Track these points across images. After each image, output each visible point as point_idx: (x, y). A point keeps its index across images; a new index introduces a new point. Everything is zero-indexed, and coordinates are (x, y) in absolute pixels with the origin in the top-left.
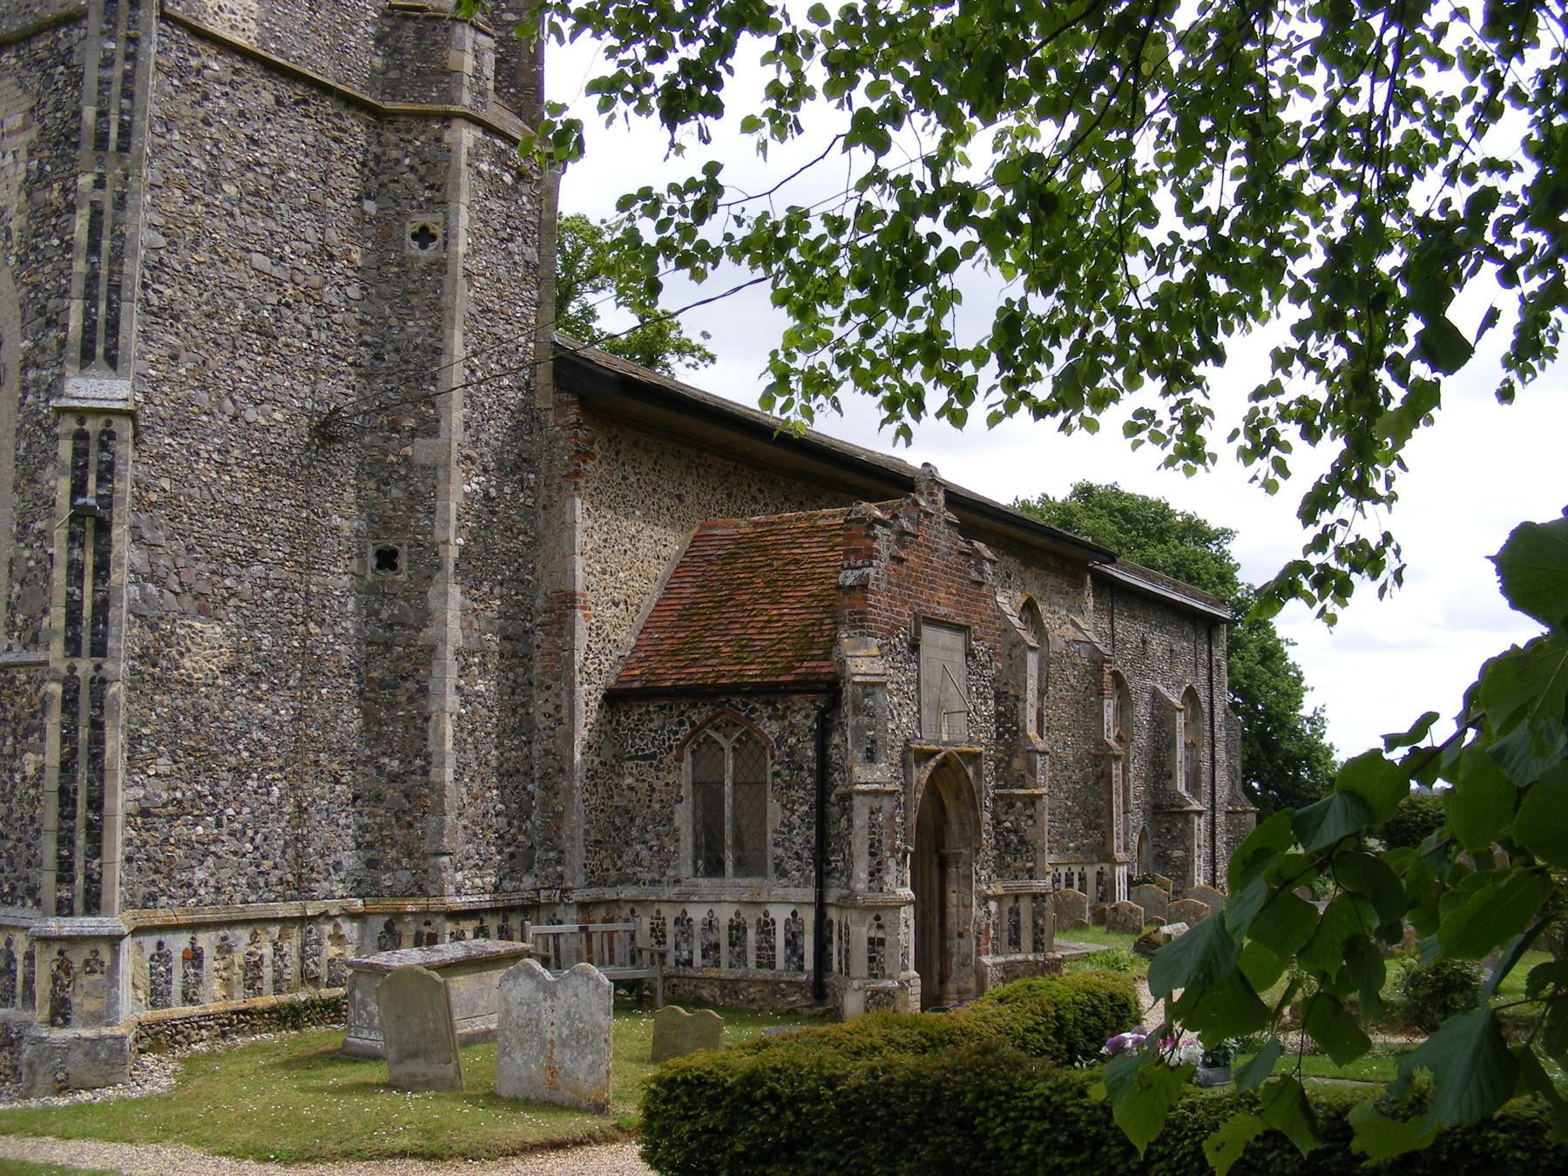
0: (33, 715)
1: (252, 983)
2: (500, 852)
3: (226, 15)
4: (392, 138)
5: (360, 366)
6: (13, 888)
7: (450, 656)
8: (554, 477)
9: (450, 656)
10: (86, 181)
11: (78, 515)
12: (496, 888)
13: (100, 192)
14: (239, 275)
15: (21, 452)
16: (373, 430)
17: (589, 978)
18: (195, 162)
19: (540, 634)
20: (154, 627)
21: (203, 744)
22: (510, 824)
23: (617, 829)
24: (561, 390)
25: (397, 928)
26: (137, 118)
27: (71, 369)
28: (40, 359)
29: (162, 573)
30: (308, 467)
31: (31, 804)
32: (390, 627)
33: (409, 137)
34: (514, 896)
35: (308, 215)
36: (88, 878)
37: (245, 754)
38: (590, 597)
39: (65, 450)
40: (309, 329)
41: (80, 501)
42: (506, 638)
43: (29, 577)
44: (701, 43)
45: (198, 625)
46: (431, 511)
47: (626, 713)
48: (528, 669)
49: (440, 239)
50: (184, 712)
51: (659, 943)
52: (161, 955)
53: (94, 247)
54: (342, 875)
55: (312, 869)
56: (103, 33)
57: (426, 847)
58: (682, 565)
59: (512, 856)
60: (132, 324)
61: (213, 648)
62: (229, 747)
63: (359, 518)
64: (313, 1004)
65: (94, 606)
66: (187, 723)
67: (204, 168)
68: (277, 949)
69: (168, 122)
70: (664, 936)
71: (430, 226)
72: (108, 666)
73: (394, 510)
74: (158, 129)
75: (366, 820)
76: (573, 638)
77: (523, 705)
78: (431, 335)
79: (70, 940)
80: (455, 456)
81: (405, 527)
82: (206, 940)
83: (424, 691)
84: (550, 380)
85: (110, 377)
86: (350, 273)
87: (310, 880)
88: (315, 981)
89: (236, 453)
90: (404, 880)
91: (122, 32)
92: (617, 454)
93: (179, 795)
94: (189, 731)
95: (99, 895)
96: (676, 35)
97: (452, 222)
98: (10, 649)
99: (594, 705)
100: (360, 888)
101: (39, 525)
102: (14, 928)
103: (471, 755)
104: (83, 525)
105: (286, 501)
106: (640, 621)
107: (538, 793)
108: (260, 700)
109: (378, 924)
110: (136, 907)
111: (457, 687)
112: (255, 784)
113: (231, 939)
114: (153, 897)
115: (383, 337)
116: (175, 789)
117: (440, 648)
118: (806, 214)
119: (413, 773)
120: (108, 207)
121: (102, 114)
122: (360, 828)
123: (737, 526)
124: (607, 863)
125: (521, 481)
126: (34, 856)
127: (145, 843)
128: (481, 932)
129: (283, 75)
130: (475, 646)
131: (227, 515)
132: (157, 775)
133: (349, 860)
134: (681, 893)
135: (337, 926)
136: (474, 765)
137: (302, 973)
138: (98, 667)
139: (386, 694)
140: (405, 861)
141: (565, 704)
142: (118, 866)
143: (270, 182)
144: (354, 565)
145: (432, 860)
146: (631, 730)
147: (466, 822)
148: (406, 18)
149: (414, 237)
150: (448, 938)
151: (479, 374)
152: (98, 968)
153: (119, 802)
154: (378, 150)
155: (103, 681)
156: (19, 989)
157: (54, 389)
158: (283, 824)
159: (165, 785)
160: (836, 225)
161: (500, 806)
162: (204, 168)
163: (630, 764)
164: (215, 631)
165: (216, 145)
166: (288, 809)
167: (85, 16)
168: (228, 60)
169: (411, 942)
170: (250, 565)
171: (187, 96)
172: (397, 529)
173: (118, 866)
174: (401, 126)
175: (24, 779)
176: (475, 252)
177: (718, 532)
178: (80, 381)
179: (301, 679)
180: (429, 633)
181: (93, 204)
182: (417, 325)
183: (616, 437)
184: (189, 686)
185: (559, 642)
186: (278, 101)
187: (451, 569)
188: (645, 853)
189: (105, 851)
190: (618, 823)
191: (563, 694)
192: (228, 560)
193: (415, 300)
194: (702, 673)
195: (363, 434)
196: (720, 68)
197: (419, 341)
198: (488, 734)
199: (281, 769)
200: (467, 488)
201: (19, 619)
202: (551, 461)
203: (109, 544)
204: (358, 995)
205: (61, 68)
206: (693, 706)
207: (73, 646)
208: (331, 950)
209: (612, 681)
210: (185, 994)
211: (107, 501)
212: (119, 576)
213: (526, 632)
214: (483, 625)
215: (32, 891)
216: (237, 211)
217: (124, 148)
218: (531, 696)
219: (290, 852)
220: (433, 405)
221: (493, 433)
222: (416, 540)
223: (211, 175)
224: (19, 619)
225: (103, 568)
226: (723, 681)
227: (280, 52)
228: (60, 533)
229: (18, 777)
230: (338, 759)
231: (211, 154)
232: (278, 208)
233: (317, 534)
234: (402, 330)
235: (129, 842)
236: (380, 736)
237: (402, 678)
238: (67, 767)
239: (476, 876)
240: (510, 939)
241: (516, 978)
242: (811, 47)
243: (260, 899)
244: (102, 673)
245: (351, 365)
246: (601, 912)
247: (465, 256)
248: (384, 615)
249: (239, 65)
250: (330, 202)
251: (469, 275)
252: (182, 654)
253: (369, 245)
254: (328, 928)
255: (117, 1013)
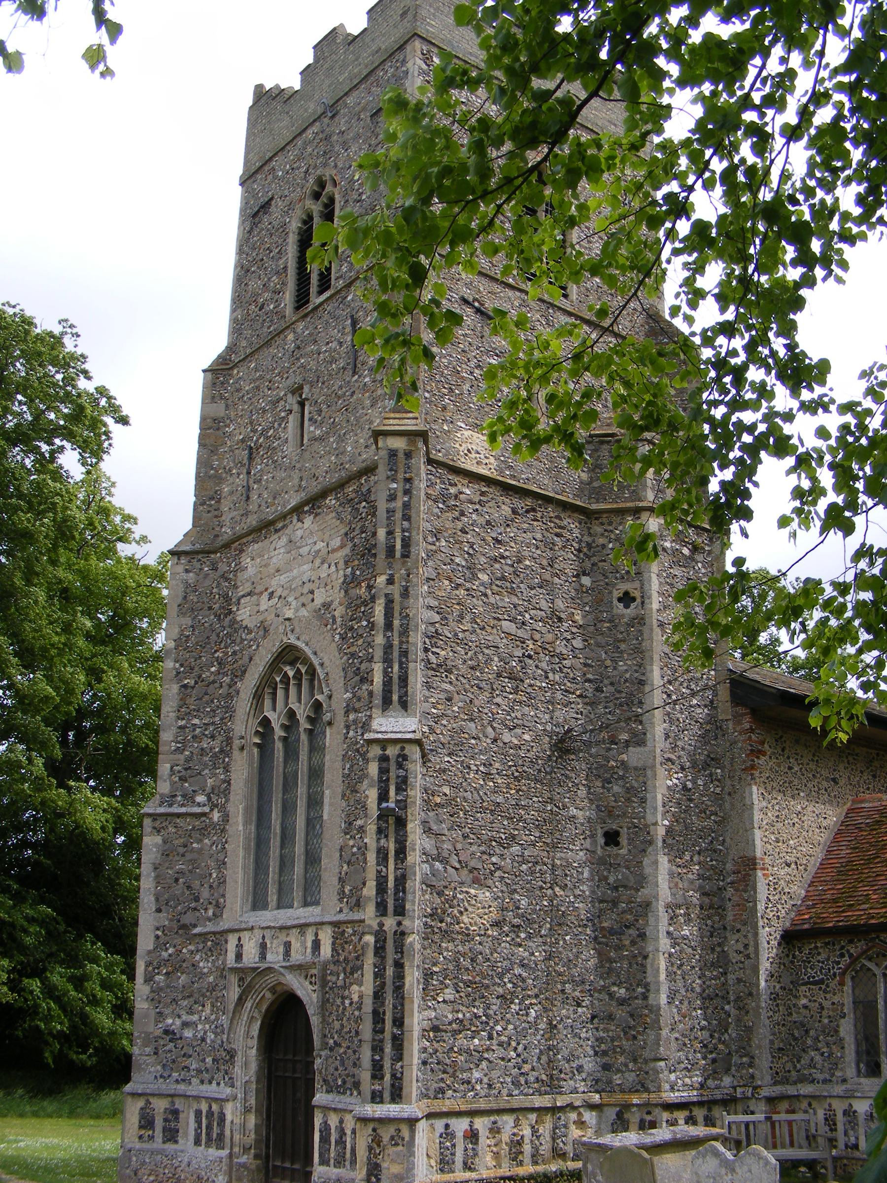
0: (357, 958)
1: (516, 1157)
2: (704, 1058)
3: (473, 455)
4: (599, 529)
5: (586, 697)
6: (344, 1082)
7: (661, 910)
8: (735, 771)
9: (661, 910)
10: (381, 580)
11: (383, 816)
12: (702, 1086)
13: (391, 587)
14: (494, 637)
15: (346, 771)
16: (598, 743)
17: (760, 1157)
18: (457, 560)
19: (730, 891)
20: (440, 894)
21: (478, 979)
22: (712, 1036)
23: (796, 1039)
24: (737, 705)
25: (625, 1116)
26: (414, 533)
27: (376, 712)
28: (357, 705)
29: (445, 854)
30: (550, 773)
31: (356, 1022)
32: (616, 888)
33: (611, 528)
34: (716, 1092)
35: (541, 591)
36: (393, 1076)
37: (509, 986)
38: (767, 860)
39: (373, 769)
40: (546, 672)
41: (384, 805)
42: (705, 894)
43: (354, 859)
44: (732, 468)
45: (472, 891)
46: (643, 801)
47: (800, 949)
48: (722, 917)
49: (639, 600)
50: (464, 955)
51: (831, 1130)
52: (448, 1134)
53: (389, 626)
54: (584, 1075)
55: (561, 1071)
56: (388, 478)
57: (647, 1054)
58: (839, 833)
59: (714, 1061)
60: (417, 677)
61: (484, 908)
62: (497, 980)
63: (590, 809)
64: (562, 1174)
65: (396, 879)
66: (466, 963)
67: (464, 563)
68: (534, 1131)
69: (437, 534)
70: (835, 1124)
71: (631, 591)
72: (406, 923)
73: (615, 801)
74: (430, 539)
75: (602, 1034)
76: (755, 892)
77: (719, 945)
78: (636, 671)
79: (381, 1121)
80: (659, 759)
81: (625, 814)
82: (481, 1124)
83: (642, 936)
84: (728, 698)
85: (403, 716)
86: (574, 630)
87: (559, 1079)
88: (563, 1156)
89: (497, 765)
90: (631, 1079)
91: (401, 476)
92: (783, 750)
93: (460, 1016)
94: (468, 969)
95: (401, 1089)
96: (715, 465)
97: (646, 587)
98: (341, 911)
99: (774, 943)
100: (597, 1086)
101: (359, 822)
102: (345, 1110)
103: (680, 984)
104: (387, 822)
105: (535, 799)
106: (808, 877)
107: (733, 1012)
108: (520, 945)
109: (611, 1114)
110: (429, 1098)
111: (668, 933)
112: (517, 1008)
113: (500, 1123)
114: (442, 1091)
115: (601, 674)
116: (457, 1012)
117: (654, 903)
118: (819, 582)
119: (636, 998)
120: (397, 597)
121: (390, 533)
122: (597, 1040)
123: (880, 800)
124: (789, 1066)
125: (711, 775)
126: (359, 1059)
127: (436, 1051)
128: (691, 1120)
129: (516, 493)
130: (680, 900)
131: (492, 811)
132: (444, 1001)
133: (589, 1064)
134: (847, 1090)
135: (580, 1114)
136: (683, 991)
137: (554, 1149)
138: (399, 924)
139: (615, 940)
140: (631, 1065)
141: (752, 943)
142: (415, 1068)
143: (512, 569)
144: (588, 844)
145: (652, 1065)
146: (804, 961)
147: (677, 1035)
148: (602, 443)
149: (620, 600)
150: (664, 1124)
151: (674, 697)
152: (400, 1142)
153: (416, 1021)
154: (589, 539)
155: (403, 934)
156: (348, 1155)
157: (366, 726)
158: (539, 1037)
159: (450, 1008)
160: (843, 588)
161: (704, 1023)
162: (464, 563)
163: (804, 988)
164: (485, 895)
165: (472, 547)
166: (542, 1026)
167: (377, 467)
168: (476, 486)
169: (637, 1127)
170: (509, 846)
171: (449, 514)
172: (618, 816)
173: (415, 1068)
174: (604, 520)
175: (351, 1004)
176: (665, 607)
177: (866, 805)
178: (382, 720)
179: (550, 929)
180: (645, 892)
181: (386, 595)
182: (626, 664)
183: (781, 737)
184: (467, 936)
185: (745, 895)
186: (514, 511)
187: (660, 844)
188: (818, 1058)
189: (405, 1056)
190: (796, 1035)
191: (750, 935)
192: (494, 843)
193: (623, 646)
194: (856, 916)
195: (591, 747)
196: (748, 485)
197: (628, 676)
198: (693, 967)
199: (537, 996)
200: (669, 783)
201: (347, 889)
202: (732, 759)
203: (405, 835)
204: (590, 1167)
205: (364, 504)
206: (851, 942)
207: (382, 909)
208: (575, 1133)
209: (788, 924)
210: (465, 1163)
211: (403, 805)
212: (414, 858)
213: (720, 889)
214: (686, 885)
215: (357, 1085)
216: (489, 592)
217: (406, 555)
218: (725, 938)
219: (544, 1058)
220: (641, 722)
221: (687, 740)
222: (633, 823)
223: (469, 568)
224: (347, 889)
225: (401, 852)
226: (873, 921)
227: (513, 477)
228: (372, 828)
229: (347, 1002)
230: (579, 989)
231: (468, 553)
232: (519, 587)
233: (559, 822)
234: (615, 668)
235: (425, 1050)
236: (611, 970)
237: (626, 927)
238: (378, 995)
239: (686, 1076)
240: (714, 1126)
241: (704, 1157)
242: (821, 458)
243: (521, 1093)
244: (402, 928)
245: (579, 696)
246: (784, 1105)
247: (658, 611)
248: (611, 880)
249: (484, 489)
250: (556, 580)
251: (661, 625)
252: (461, 913)
253: (587, 609)
254: (573, 1116)
255: (413, 1176)
